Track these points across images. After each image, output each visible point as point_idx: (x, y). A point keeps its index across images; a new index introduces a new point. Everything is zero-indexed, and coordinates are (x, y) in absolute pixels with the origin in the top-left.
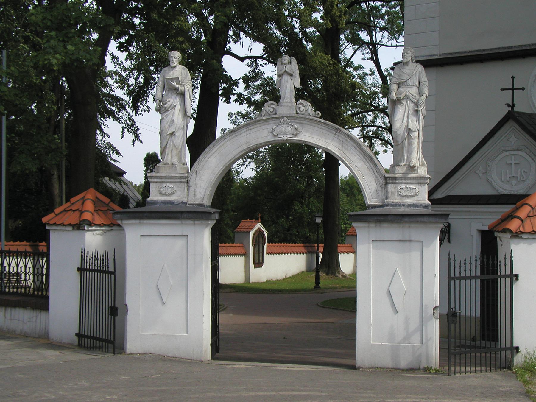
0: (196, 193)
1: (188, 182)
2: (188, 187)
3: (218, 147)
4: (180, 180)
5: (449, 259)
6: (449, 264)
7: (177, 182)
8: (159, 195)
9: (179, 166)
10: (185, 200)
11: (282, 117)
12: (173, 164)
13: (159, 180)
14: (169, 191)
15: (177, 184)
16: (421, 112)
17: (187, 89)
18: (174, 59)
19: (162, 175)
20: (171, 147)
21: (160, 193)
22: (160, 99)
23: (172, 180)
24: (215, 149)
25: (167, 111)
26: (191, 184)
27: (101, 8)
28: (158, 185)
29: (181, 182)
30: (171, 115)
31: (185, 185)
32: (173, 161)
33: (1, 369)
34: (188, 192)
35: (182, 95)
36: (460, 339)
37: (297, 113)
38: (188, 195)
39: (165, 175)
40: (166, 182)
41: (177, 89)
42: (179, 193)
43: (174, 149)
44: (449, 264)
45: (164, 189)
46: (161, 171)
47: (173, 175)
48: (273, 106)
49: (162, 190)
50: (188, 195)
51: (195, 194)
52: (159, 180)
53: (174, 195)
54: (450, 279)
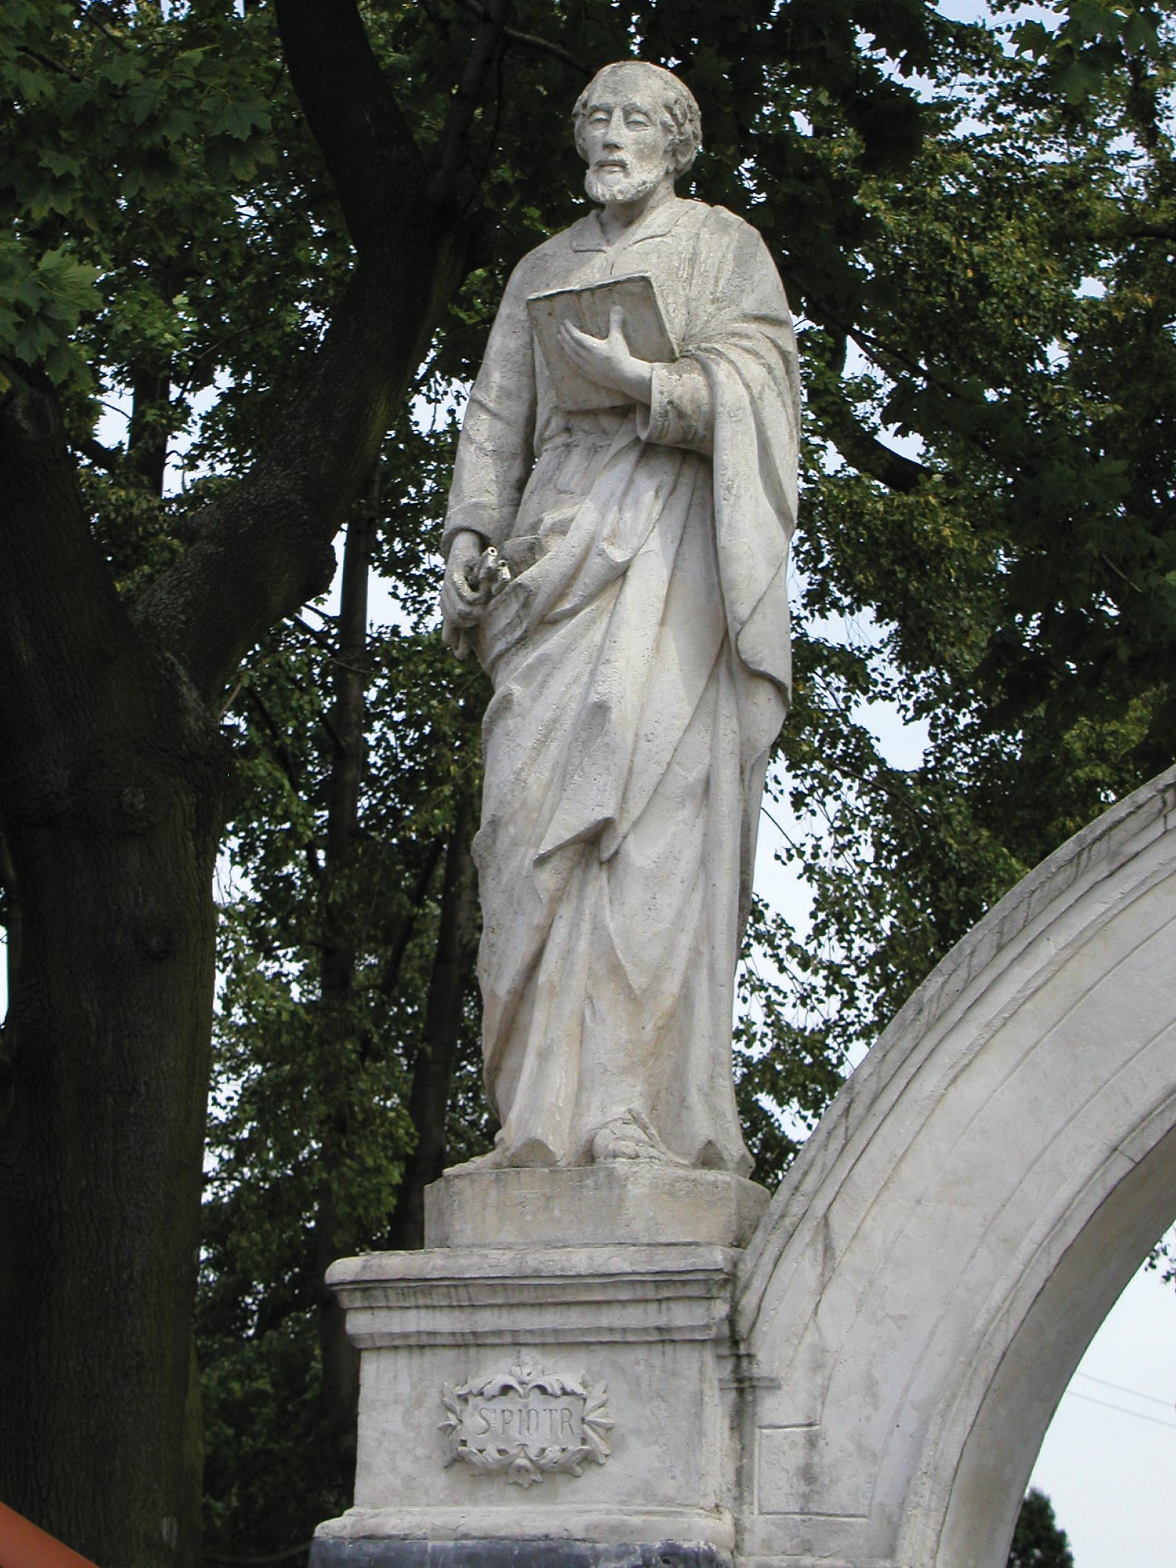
0: (828, 1455)
1: (734, 1342)
2: (745, 1389)
3: (1048, 950)
4: (653, 1317)
7: (618, 1342)
8: (440, 1481)
9: (645, 1172)
12: (589, 1155)
13: (443, 1322)
14: (543, 1435)
15: (626, 1357)
17: (731, 392)
18: (619, 132)
19: (468, 1264)
20: (579, 983)
21: (457, 1461)
22: (487, 522)
23: (574, 1319)
24: (1021, 976)
25: (547, 622)
26: (769, 1356)
27: (312, 1224)
28: (438, 1374)
29: (665, 1338)
30: (576, 664)
31: (704, 1374)
32: (591, 1120)
33: (158, 4)
34: (743, 1450)
35: (686, 452)
38: (742, 1481)
39: (499, 1262)
40: (515, 1342)
41: (629, 404)
42: (637, 1460)
43: (607, 997)
45: (493, 1411)
46: (464, 1227)
47: (580, 1260)
49: (473, 1421)
50: (742, 1481)
51: (808, 1474)
52: (443, 1322)
53: (590, 1480)
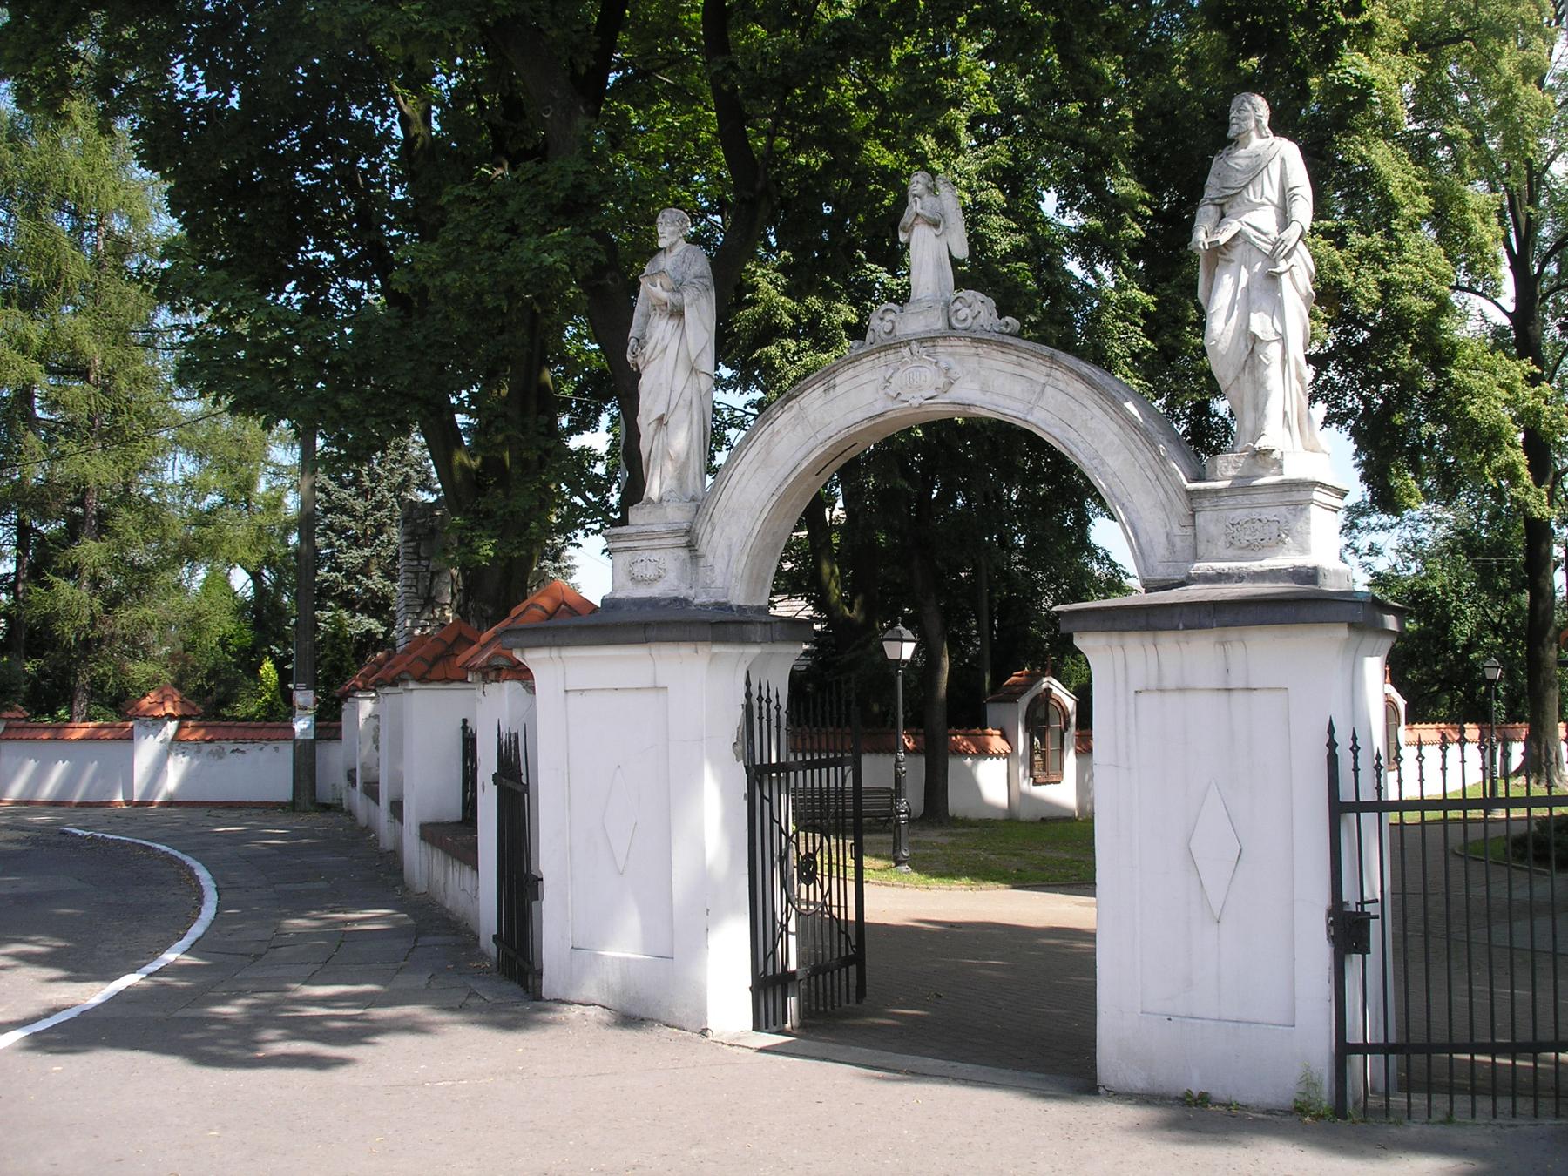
5: (1332, 745)
6: (1332, 760)
10: (683, 592)
11: (908, 343)
14: (650, 573)
16: (1285, 278)
23: (656, 542)
36: (1511, 948)
37: (951, 327)
44: (1332, 760)
48: (890, 316)
54: (1338, 809)
